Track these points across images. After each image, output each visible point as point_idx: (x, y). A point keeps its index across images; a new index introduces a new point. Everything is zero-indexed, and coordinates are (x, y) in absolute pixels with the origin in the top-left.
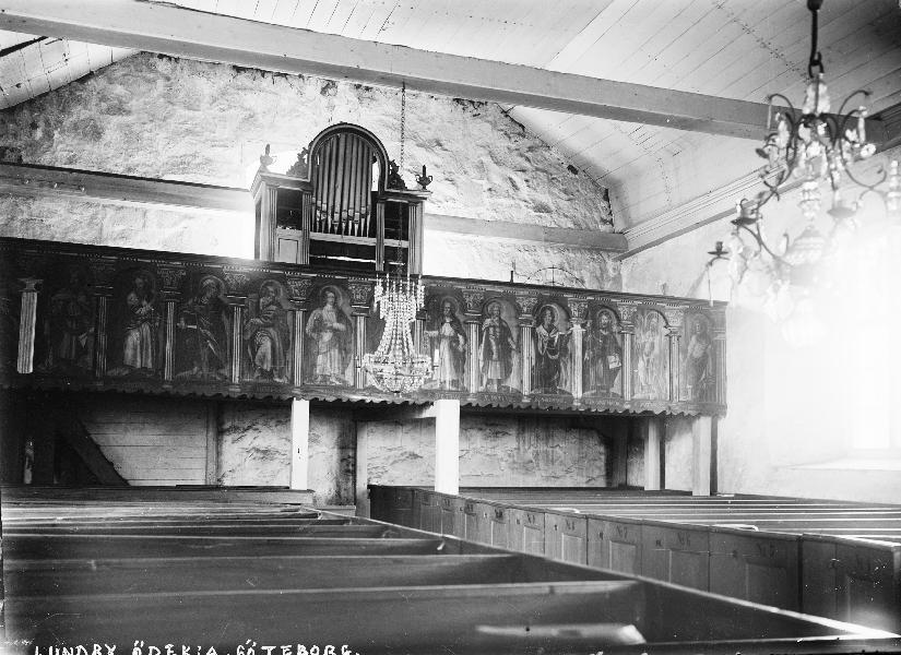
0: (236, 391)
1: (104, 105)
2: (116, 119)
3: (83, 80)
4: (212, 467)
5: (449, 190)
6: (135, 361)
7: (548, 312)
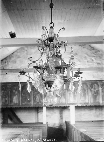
0: (32, 106)
1: (16, 57)
2: (19, 59)
3: (13, 53)
4: (37, 119)
5: (79, 63)
6: (15, 102)
7: (94, 86)
